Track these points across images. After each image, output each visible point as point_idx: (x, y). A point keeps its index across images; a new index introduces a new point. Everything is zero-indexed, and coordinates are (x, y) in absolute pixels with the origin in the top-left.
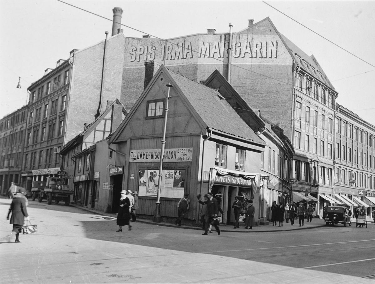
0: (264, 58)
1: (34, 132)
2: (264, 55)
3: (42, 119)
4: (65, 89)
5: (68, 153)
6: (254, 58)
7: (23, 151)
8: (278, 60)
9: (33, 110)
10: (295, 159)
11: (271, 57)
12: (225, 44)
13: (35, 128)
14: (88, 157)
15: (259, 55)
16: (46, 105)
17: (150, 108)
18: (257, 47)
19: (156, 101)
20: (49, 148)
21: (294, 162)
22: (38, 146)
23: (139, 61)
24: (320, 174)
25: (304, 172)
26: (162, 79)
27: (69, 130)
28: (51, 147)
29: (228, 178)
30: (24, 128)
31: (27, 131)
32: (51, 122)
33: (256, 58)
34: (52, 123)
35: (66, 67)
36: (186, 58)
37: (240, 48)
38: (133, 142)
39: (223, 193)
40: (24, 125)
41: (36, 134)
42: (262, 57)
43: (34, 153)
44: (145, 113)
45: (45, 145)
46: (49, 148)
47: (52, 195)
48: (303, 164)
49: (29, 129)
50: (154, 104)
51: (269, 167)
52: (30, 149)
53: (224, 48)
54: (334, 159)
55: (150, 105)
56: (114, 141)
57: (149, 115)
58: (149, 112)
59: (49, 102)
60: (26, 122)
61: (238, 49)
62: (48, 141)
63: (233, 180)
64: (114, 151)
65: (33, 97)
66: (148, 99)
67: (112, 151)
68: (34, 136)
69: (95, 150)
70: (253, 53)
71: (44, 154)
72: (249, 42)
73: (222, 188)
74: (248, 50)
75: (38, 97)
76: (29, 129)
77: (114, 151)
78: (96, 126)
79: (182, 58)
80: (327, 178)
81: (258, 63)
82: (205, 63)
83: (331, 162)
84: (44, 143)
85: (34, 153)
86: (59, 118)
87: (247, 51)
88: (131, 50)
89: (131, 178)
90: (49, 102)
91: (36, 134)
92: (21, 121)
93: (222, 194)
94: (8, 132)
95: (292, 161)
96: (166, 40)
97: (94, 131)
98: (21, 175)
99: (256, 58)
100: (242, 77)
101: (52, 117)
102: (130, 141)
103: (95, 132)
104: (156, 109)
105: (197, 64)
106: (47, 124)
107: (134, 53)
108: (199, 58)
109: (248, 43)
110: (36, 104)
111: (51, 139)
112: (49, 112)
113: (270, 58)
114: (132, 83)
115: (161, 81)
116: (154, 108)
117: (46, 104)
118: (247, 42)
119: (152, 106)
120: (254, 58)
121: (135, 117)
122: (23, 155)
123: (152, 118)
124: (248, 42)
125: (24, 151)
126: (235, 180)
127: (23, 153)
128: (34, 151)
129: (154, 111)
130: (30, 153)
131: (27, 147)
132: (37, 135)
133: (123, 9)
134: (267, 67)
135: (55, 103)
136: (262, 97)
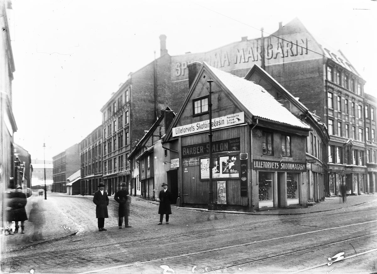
0: (296, 55)
1: (109, 144)
2: (295, 53)
3: (112, 133)
4: (126, 106)
5: (134, 159)
6: (286, 57)
7: (103, 160)
8: (308, 56)
9: (106, 127)
10: (330, 145)
11: (302, 54)
12: (257, 48)
13: (109, 141)
14: (149, 158)
15: (290, 53)
16: (114, 122)
17: (196, 106)
18: (287, 47)
19: (201, 99)
20: (120, 155)
21: (329, 147)
22: (113, 155)
23: (184, 75)
24: (353, 157)
25: (339, 156)
26: (204, 77)
27: (134, 139)
28: (122, 155)
29: (276, 164)
30: (101, 142)
31: (103, 145)
32: (119, 135)
33: (287, 56)
34: (120, 135)
35: (125, 88)
36: (223, 66)
37: (272, 49)
38: (183, 139)
39: (272, 179)
40: (101, 140)
41: (110, 146)
42: (293, 55)
43: (110, 161)
44: (192, 111)
45: (117, 153)
46: (120, 155)
47: (265, 209)
48: (337, 149)
49: (105, 143)
50: (199, 101)
51: (312, 152)
52: (107, 158)
53: (257, 51)
54: (365, 142)
55: (196, 103)
56: (167, 140)
57: (196, 113)
58: (196, 109)
59: (116, 119)
60: (102, 138)
61: (270, 51)
62: (119, 150)
63: (282, 165)
64: (168, 149)
65: (105, 116)
66: (192, 98)
67: (165, 149)
68: (109, 147)
69: (153, 152)
70: (284, 53)
71: (117, 161)
72: (280, 43)
73: (271, 175)
74: (280, 50)
75: (108, 116)
76: (105, 143)
77: (168, 149)
78: (153, 132)
79: (220, 66)
80: (360, 160)
81: (290, 61)
82: (241, 68)
83: (363, 145)
84: (117, 152)
85: (110, 161)
86: (125, 131)
87: (278, 51)
88: (176, 67)
89: (185, 172)
90: (116, 119)
91: (110, 146)
92: (99, 137)
93: (271, 180)
94: (91, 147)
95: (328, 146)
96: (205, 53)
97: (151, 137)
98: (103, 179)
99: (287, 56)
100: (276, 76)
101: (120, 131)
102: (181, 139)
103: (153, 137)
104: (201, 106)
105: (195, 267)
106: (117, 136)
107: (179, 69)
108: (236, 64)
109: (280, 44)
110: (107, 122)
111: (121, 148)
112: (117, 127)
113: (301, 55)
114: (180, 94)
115: (203, 78)
116: (200, 105)
117: (114, 121)
118: (278, 43)
119: (197, 104)
120: (286, 57)
121: (183, 116)
122: (103, 163)
123: (199, 115)
124: (279, 43)
125: (103, 160)
126: (284, 166)
127: (103, 161)
128: (110, 159)
129: (200, 108)
130: (107, 160)
131: (105, 157)
132: (111, 146)
133: (166, 35)
134: (299, 64)
135: (120, 119)
136: (296, 92)
